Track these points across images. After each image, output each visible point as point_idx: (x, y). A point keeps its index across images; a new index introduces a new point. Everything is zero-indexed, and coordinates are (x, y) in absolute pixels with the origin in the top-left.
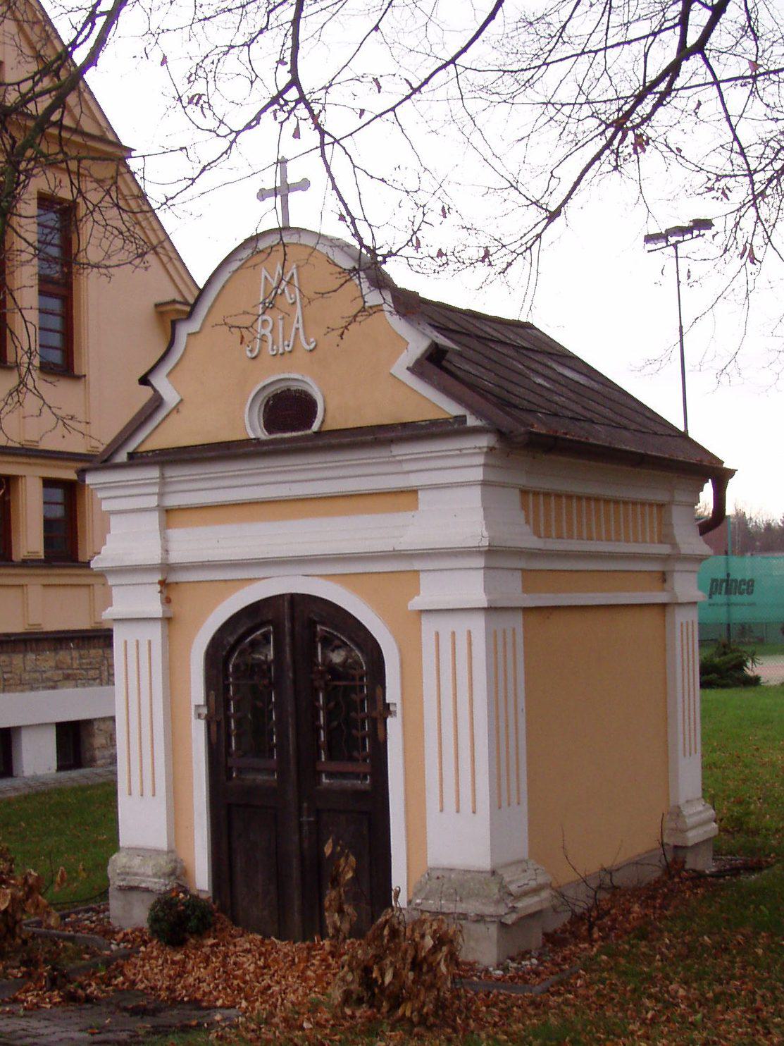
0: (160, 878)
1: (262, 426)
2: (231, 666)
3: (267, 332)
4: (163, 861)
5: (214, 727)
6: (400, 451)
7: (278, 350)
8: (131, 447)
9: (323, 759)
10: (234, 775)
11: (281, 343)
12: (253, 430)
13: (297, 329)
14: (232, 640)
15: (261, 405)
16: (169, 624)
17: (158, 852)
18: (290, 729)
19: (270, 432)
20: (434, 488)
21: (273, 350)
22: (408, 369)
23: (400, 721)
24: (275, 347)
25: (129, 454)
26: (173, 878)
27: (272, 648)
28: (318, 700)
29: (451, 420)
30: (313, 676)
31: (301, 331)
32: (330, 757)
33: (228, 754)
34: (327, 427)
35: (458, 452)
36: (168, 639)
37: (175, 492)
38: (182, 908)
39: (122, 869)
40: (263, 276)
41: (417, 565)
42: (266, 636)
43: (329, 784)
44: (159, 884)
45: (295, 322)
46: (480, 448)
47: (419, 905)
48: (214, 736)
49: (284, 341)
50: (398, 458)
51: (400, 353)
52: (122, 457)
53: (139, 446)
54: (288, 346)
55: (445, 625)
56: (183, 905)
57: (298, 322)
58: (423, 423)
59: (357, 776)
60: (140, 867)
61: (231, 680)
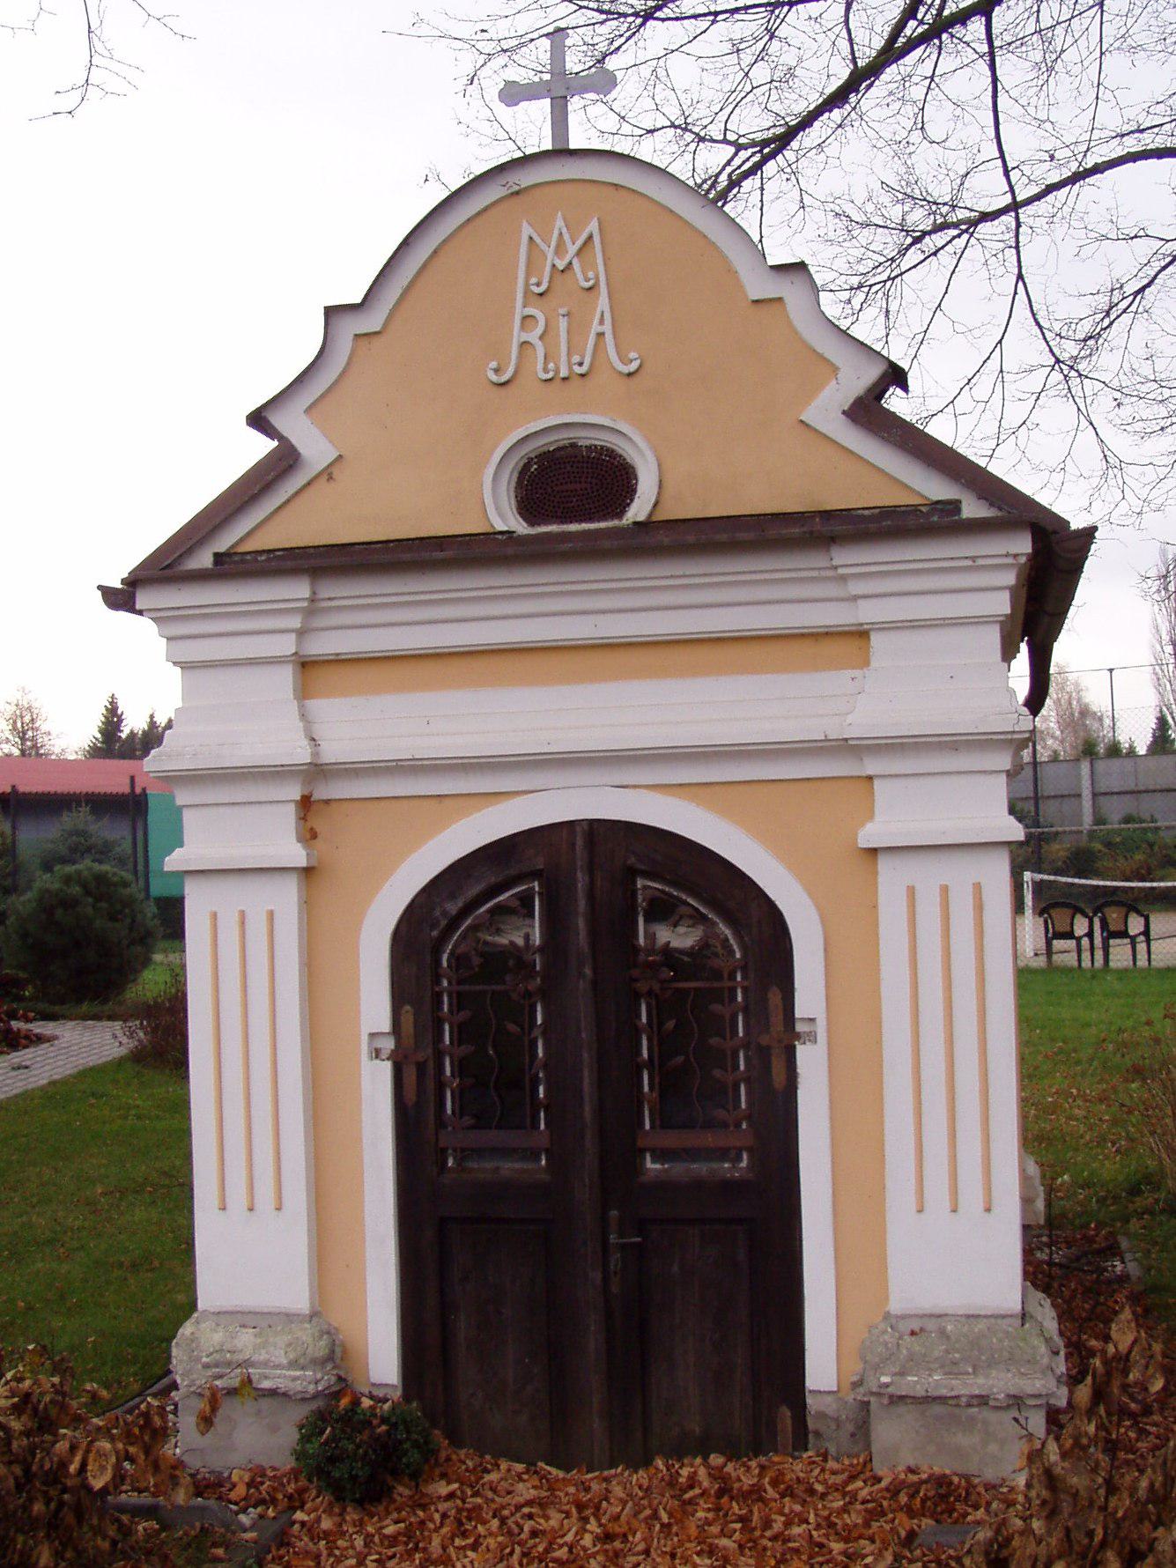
0: (303, 1368)
1: (515, 510)
2: (445, 957)
3: (533, 337)
4: (306, 1333)
5: (410, 1075)
6: (847, 557)
7: (557, 371)
8: (224, 543)
9: (647, 1127)
10: (450, 1163)
11: (564, 358)
12: (502, 516)
13: (601, 335)
14: (453, 908)
15: (512, 473)
16: (307, 877)
17: (289, 1317)
18: (586, 1073)
19: (532, 524)
20: (231, 665)
21: (546, 370)
22: (844, 412)
23: (825, 1048)
24: (551, 366)
25: (217, 556)
26: (329, 1366)
27: (537, 924)
28: (639, 1016)
29: (924, 509)
30: (635, 973)
31: (609, 337)
32: (664, 1121)
33: (441, 1122)
34: (671, 512)
35: (969, 563)
36: (308, 906)
37: (323, 629)
38: (384, 1428)
39: (217, 1356)
40: (525, 240)
41: (871, 766)
42: (526, 901)
43: (660, 1171)
44: (306, 1381)
45: (596, 321)
46: (1015, 556)
47: (887, 1385)
48: (410, 1095)
49: (569, 355)
50: (840, 571)
51: (818, 388)
52: (204, 560)
53: (242, 540)
54: (581, 364)
55: (929, 875)
56: (384, 1420)
57: (602, 322)
58: (866, 512)
59: (723, 1154)
60: (256, 1348)
61: (445, 983)
